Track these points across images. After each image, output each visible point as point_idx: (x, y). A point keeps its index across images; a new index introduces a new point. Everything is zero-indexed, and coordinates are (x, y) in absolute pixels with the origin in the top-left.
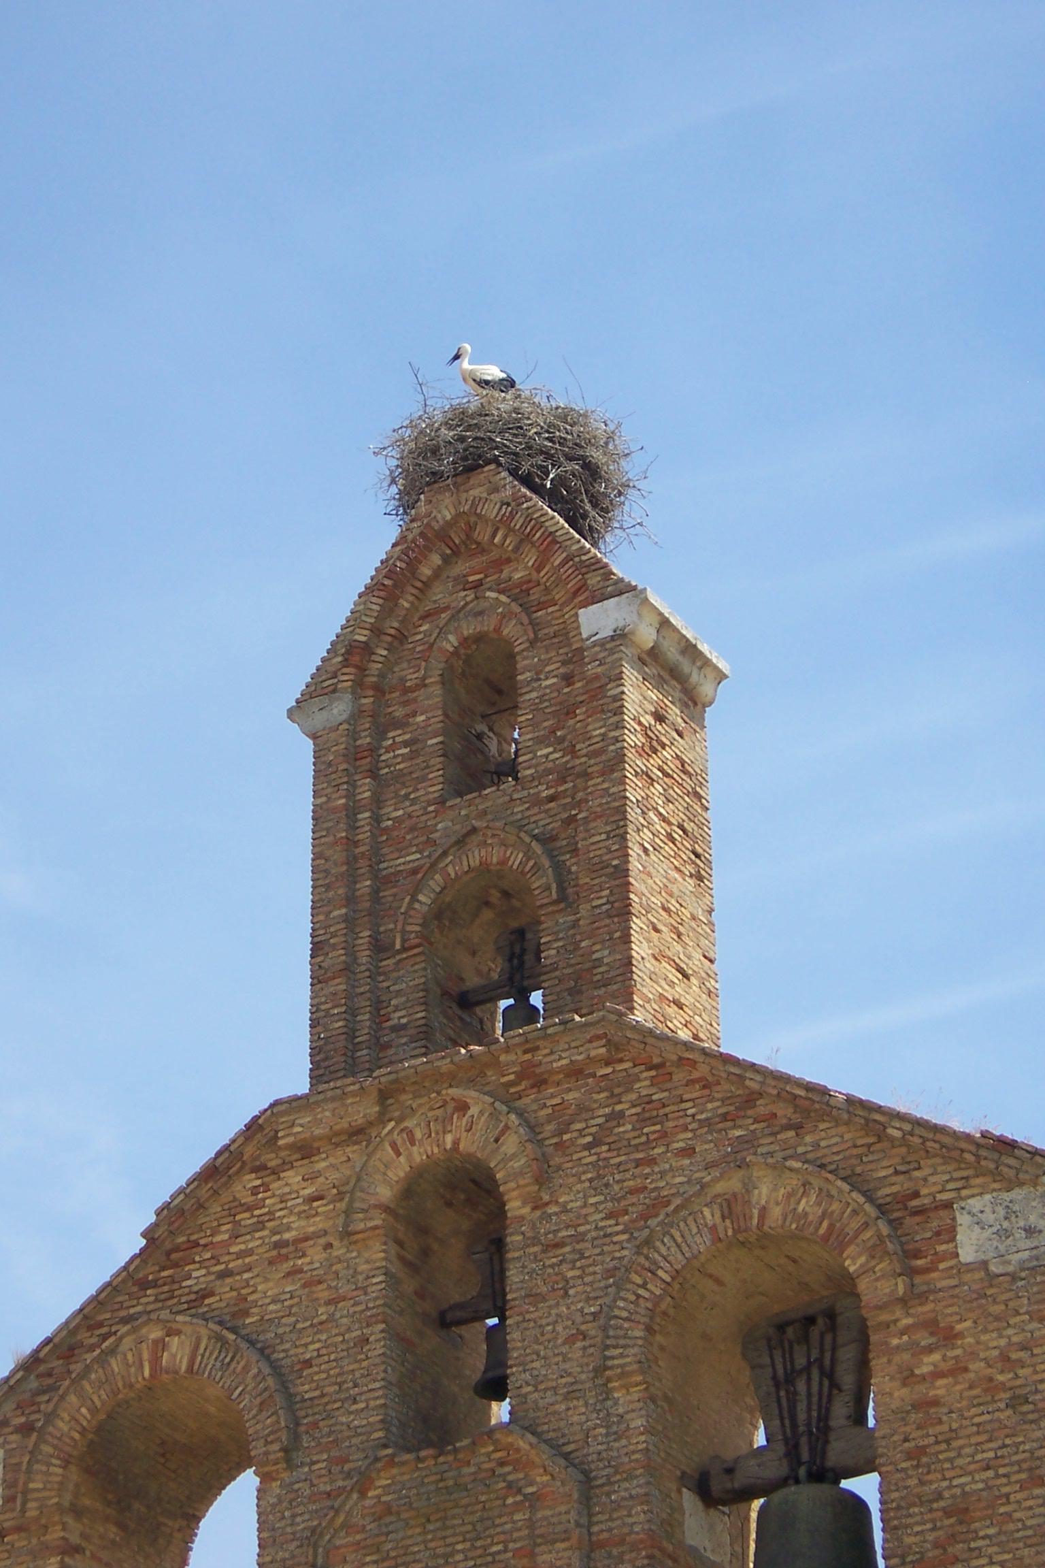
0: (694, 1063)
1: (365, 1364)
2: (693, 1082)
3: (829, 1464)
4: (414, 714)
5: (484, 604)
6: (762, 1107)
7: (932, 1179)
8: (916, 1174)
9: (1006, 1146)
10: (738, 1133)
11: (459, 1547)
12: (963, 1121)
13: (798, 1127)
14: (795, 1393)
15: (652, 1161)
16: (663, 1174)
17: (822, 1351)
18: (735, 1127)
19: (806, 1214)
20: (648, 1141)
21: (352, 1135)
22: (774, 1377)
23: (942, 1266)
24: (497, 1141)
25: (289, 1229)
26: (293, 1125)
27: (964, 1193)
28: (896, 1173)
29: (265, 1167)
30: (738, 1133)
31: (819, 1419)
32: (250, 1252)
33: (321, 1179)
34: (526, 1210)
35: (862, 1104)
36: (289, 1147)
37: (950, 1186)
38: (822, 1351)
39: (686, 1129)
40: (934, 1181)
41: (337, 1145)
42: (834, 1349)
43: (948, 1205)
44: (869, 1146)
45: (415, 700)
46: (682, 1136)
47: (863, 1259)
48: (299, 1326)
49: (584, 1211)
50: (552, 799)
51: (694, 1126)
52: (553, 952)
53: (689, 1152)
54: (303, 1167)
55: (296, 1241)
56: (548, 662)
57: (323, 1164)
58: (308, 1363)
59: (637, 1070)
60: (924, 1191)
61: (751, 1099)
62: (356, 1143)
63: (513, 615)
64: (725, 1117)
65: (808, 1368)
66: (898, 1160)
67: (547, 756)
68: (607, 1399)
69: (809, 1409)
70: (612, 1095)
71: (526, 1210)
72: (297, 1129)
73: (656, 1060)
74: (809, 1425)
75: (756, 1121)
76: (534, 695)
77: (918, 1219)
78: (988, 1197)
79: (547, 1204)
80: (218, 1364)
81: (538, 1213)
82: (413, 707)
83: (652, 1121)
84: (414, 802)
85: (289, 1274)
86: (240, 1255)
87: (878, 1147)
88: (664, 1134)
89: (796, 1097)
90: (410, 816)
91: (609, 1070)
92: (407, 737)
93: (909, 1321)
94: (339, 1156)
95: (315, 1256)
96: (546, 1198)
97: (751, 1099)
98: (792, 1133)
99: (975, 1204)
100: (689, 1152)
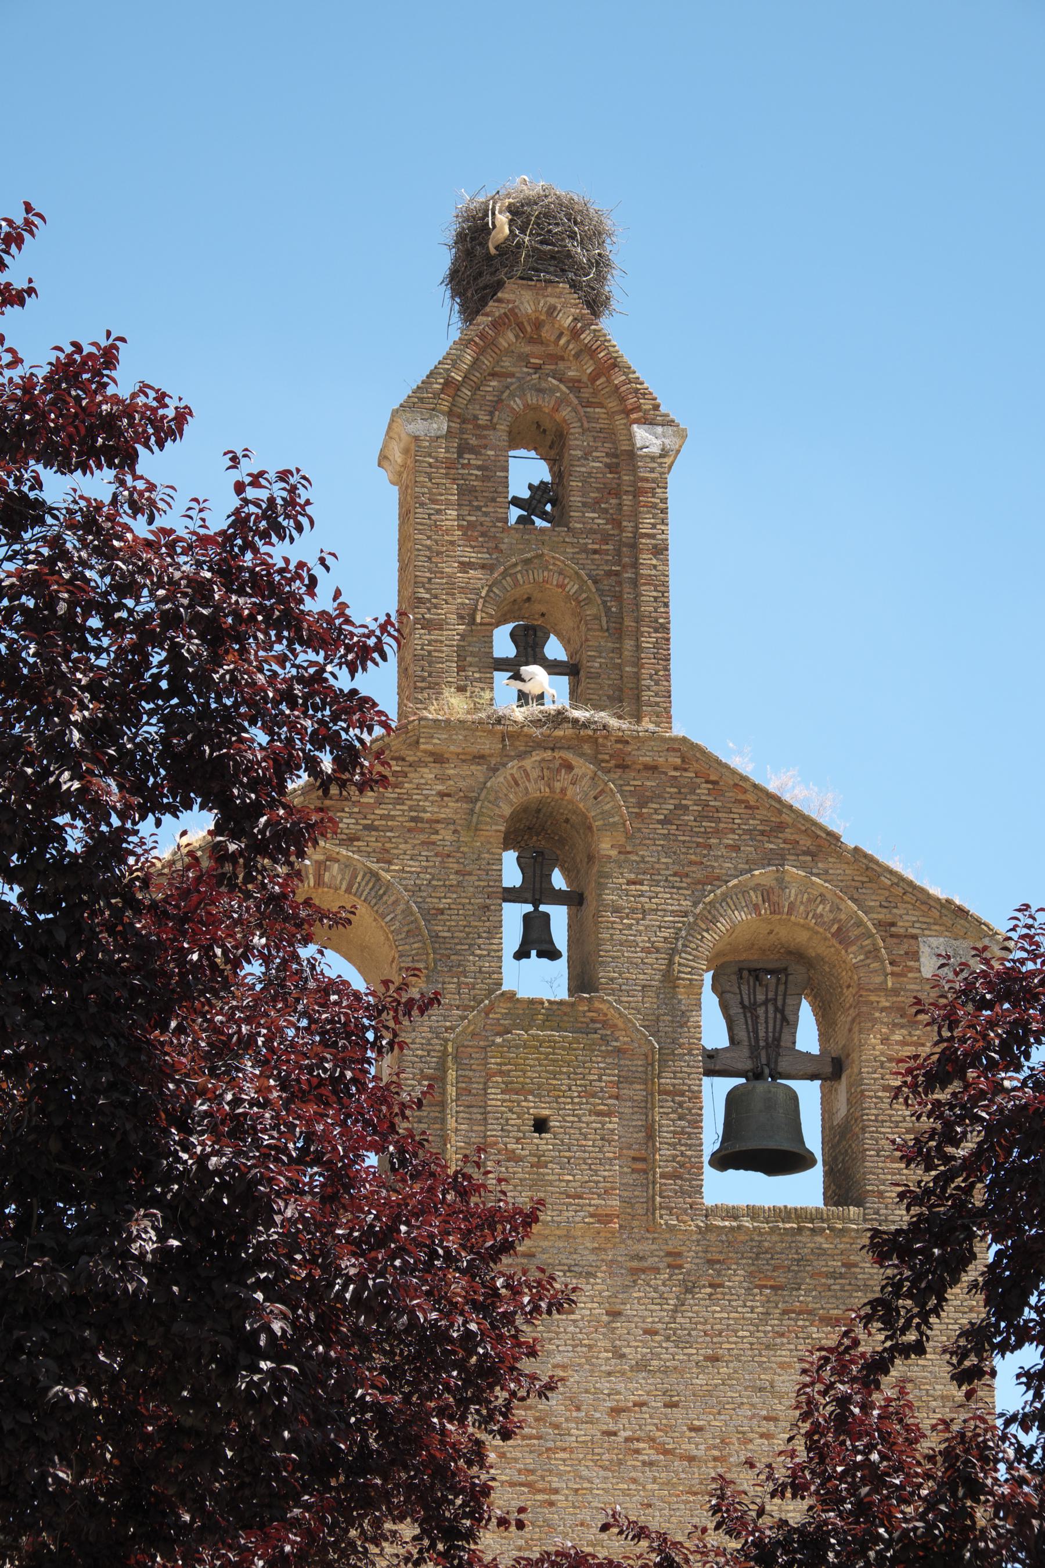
0: (745, 791)
1: (487, 924)
2: (741, 802)
3: (780, 1070)
4: (485, 447)
5: (544, 385)
6: (788, 834)
7: (905, 917)
8: (895, 911)
9: (961, 912)
10: (772, 846)
11: (565, 1070)
12: (937, 891)
13: (813, 855)
14: (757, 1017)
15: (710, 847)
16: (716, 858)
17: (776, 994)
18: (770, 842)
19: (822, 915)
20: (705, 832)
21: (475, 757)
22: (742, 1003)
23: (910, 975)
24: (595, 798)
25: (426, 812)
26: (432, 737)
27: (927, 932)
28: (881, 906)
29: (403, 760)
30: (772, 846)
31: (774, 1039)
32: (393, 818)
33: (451, 783)
34: (614, 853)
35: (866, 856)
36: (425, 751)
37: (917, 925)
38: (776, 994)
39: (733, 831)
40: (907, 919)
41: (464, 761)
42: (785, 995)
43: (915, 937)
44: (863, 883)
45: (485, 437)
46: (731, 836)
47: (862, 957)
48: (434, 883)
49: (657, 866)
50: (595, 552)
51: (740, 832)
52: (597, 665)
53: (736, 848)
54: (436, 769)
55: (429, 821)
56: (596, 449)
57: (452, 772)
58: (442, 912)
59: (698, 780)
60: (900, 924)
61: (781, 827)
62: (479, 764)
63: (569, 404)
64: (762, 833)
65: (766, 1003)
66: (882, 898)
67: (593, 519)
68: (673, 998)
69: (767, 1032)
70: (680, 793)
71: (614, 853)
72: (436, 741)
73: (713, 778)
74: (766, 1040)
75: (785, 842)
76: (583, 469)
77: (895, 940)
78: (942, 939)
79: (629, 853)
80: (373, 893)
81: (622, 857)
82: (484, 441)
83: (710, 819)
84: (486, 514)
85: (423, 843)
86: (382, 817)
87: (869, 885)
88: (717, 831)
89: (818, 836)
90: (482, 524)
91: (678, 774)
92: (480, 463)
93: (887, 1004)
94: (466, 770)
95: (446, 835)
96: (629, 849)
97: (781, 827)
98: (809, 858)
99: (934, 941)
100: (736, 848)
